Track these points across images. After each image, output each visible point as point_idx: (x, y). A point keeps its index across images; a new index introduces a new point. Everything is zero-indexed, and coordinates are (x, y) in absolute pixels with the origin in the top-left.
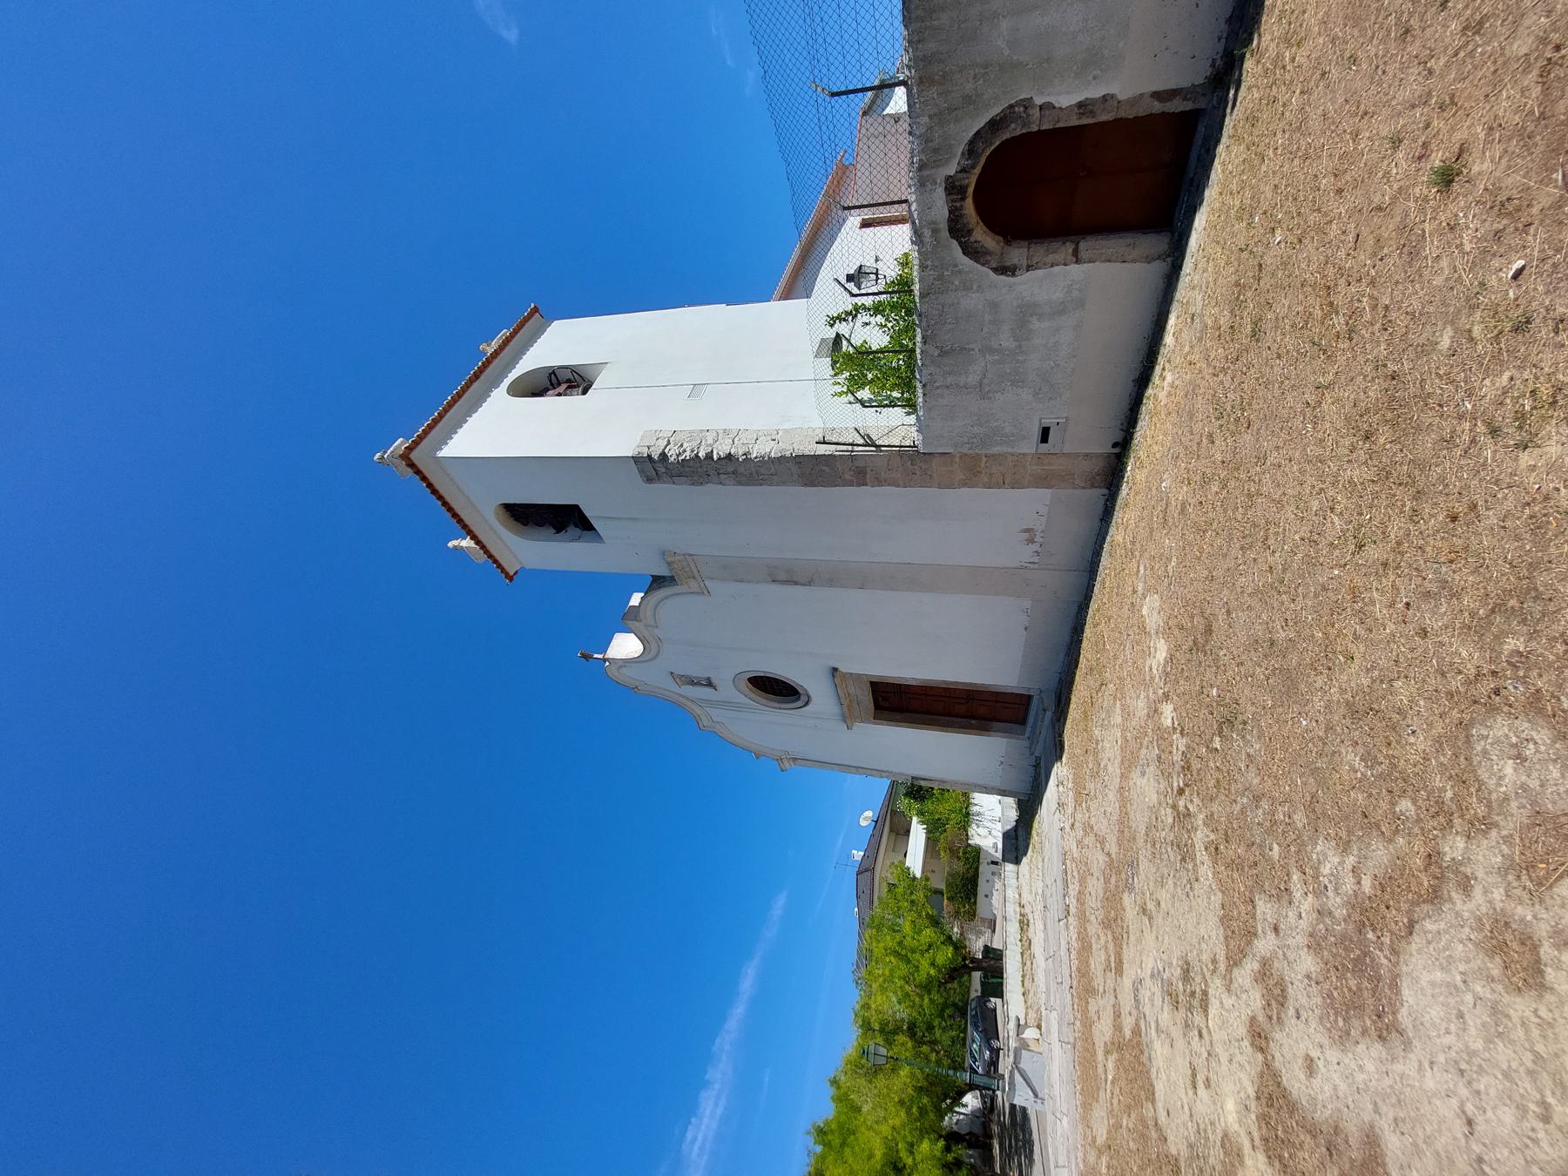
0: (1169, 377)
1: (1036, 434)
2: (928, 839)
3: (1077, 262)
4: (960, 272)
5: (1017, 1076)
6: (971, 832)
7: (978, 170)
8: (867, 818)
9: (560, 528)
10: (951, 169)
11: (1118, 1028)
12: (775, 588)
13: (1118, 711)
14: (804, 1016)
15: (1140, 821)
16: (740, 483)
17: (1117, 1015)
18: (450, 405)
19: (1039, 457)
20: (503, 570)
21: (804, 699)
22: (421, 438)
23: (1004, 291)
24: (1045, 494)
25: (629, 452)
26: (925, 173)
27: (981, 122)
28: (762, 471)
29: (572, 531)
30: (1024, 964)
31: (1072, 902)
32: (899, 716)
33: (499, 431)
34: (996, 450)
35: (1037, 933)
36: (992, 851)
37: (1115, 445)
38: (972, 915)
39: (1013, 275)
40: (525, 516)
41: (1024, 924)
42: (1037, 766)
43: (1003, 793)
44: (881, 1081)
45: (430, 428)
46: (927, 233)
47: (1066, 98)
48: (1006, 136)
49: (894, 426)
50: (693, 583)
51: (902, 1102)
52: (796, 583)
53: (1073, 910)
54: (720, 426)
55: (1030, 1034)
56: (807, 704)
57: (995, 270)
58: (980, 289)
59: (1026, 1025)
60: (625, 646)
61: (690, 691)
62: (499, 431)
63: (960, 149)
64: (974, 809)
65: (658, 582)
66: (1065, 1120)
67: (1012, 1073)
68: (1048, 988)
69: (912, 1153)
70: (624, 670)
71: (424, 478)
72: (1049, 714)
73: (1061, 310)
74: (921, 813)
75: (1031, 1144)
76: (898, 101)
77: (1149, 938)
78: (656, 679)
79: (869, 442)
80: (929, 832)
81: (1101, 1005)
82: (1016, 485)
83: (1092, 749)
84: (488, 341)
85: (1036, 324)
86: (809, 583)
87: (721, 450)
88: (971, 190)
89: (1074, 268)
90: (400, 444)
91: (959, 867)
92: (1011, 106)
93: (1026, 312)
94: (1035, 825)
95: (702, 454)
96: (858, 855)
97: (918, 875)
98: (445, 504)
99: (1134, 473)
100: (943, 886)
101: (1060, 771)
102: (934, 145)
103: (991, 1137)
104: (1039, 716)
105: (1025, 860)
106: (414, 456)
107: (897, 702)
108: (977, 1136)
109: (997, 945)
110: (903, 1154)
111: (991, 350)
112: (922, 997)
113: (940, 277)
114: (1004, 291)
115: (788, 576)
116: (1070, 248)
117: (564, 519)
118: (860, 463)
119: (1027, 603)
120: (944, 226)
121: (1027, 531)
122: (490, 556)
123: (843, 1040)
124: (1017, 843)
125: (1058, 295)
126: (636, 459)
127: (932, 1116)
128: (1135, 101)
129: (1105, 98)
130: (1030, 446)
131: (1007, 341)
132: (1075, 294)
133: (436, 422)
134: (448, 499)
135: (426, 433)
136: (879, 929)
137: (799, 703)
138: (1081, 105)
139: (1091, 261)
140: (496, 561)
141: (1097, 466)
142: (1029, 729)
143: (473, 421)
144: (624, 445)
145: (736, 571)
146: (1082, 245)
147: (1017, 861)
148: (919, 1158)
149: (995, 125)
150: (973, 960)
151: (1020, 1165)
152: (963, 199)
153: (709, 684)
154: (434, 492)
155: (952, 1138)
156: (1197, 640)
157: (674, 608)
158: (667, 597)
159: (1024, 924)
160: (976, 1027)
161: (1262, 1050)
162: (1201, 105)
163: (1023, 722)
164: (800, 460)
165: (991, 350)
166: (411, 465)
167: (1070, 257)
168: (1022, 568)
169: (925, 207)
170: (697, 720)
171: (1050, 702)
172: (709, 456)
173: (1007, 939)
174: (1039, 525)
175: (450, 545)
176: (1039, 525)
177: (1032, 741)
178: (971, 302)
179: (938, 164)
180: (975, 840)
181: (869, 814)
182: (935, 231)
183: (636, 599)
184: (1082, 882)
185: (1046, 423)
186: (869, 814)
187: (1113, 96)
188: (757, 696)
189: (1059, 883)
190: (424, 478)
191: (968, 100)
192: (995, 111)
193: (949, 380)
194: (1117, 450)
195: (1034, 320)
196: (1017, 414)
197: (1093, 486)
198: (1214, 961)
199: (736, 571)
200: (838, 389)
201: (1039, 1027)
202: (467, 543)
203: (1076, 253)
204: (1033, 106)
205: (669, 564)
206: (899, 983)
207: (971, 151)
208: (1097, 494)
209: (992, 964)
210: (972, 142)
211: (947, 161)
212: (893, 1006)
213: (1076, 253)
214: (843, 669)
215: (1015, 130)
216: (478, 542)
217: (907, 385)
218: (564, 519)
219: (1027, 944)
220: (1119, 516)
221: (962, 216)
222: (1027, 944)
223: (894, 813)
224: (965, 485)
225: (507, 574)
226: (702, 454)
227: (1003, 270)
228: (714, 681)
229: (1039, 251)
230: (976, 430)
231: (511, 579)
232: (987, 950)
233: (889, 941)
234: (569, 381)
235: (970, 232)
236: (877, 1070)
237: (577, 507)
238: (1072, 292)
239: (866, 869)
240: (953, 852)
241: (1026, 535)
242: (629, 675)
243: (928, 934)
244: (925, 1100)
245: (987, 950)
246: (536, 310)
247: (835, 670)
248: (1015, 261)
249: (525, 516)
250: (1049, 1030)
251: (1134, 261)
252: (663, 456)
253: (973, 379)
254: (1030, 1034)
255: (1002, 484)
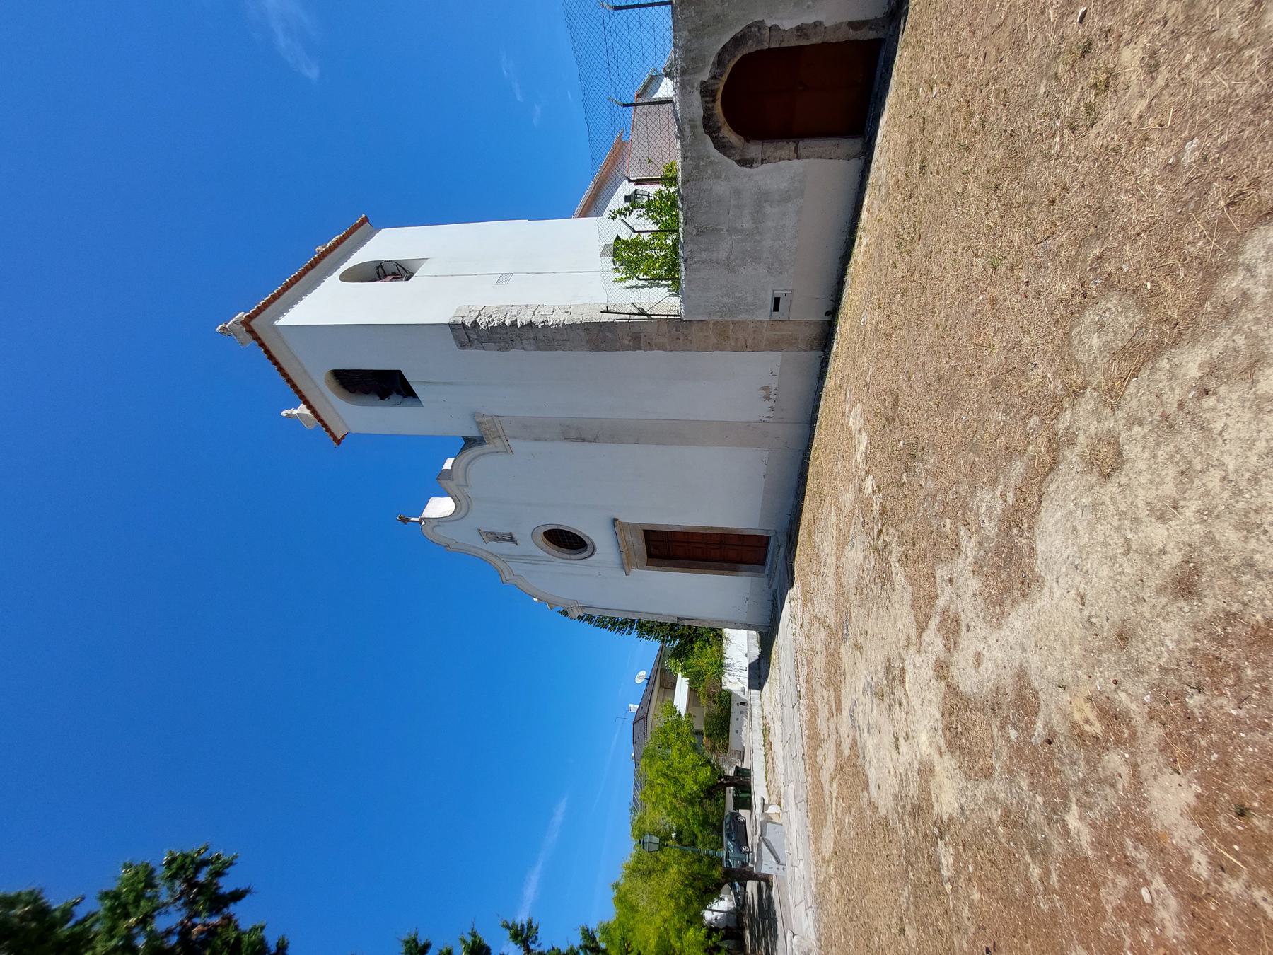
0: (864, 241)
1: (770, 304)
2: (691, 690)
3: (798, 157)
4: (712, 162)
5: (764, 847)
6: (724, 680)
7: (725, 78)
8: (641, 677)
9: (383, 395)
10: (705, 76)
11: (839, 754)
12: (567, 445)
13: (834, 513)
14: (588, 851)
15: (850, 582)
16: (539, 349)
17: (839, 744)
18: (288, 286)
19: (773, 323)
20: (332, 434)
21: (590, 549)
22: (260, 310)
23: (745, 180)
24: (775, 357)
25: (446, 320)
26: (686, 78)
27: (726, 39)
28: (558, 337)
29: (395, 398)
30: (767, 763)
31: (803, 688)
32: (667, 562)
33: (330, 304)
34: (741, 317)
35: (776, 738)
36: (741, 694)
37: (827, 314)
38: (726, 748)
39: (752, 167)
40: (355, 382)
41: (766, 731)
42: (774, 600)
43: (748, 627)
44: (654, 881)
45: (269, 302)
46: (687, 128)
47: (788, 24)
48: (746, 51)
49: (660, 300)
50: (498, 442)
51: (671, 896)
52: (583, 440)
53: (803, 692)
54: (523, 303)
55: (772, 810)
56: (592, 554)
57: (738, 162)
58: (727, 178)
59: (769, 804)
60: (440, 507)
61: (495, 547)
62: (330, 304)
63: (712, 59)
64: (726, 662)
65: (469, 442)
66: (801, 866)
67: (759, 845)
68: (785, 770)
69: (680, 938)
70: (437, 529)
71: (262, 345)
72: (782, 550)
73: (786, 199)
74: (684, 669)
75: (775, 921)
76: (666, 89)
77: (861, 665)
78: (465, 537)
79: (642, 313)
80: (691, 683)
81: (828, 750)
82: (756, 348)
83: (816, 558)
84: (323, 244)
85: (769, 209)
86: (595, 440)
87: (524, 319)
88: (719, 94)
89: (796, 162)
90: (241, 315)
91: (715, 708)
92: (749, 26)
93: (762, 198)
94: (773, 656)
95: (507, 322)
96: (634, 707)
97: (683, 712)
98: (280, 369)
99: (843, 328)
100: (702, 728)
101: (794, 592)
102: (691, 55)
103: (743, 929)
104: (775, 554)
105: (766, 686)
106: (254, 323)
107: (668, 548)
108: (732, 929)
109: (745, 766)
110: (673, 941)
111: (736, 231)
112: (687, 809)
113: (697, 167)
114: (745, 180)
115: (577, 434)
116: (792, 146)
117: (386, 385)
118: (636, 330)
119: (766, 453)
120: (700, 123)
121: (764, 389)
122: (320, 420)
123: (622, 849)
124: (759, 673)
125: (784, 185)
126: (452, 326)
127: (696, 904)
128: (837, 27)
129: (816, 24)
130: (765, 314)
131: (748, 225)
132: (797, 184)
133: (275, 298)
134: (283, 365)
135: (265, 306)
136: (652, 757)
137: (587, 554)
138: (798, 29)
139: (808, 157)
140: (325, 425)
141: (811, 332)
142: (768, 567)
143: (308, 299)
144: (442, 313)
145: (534, 430)
146: (801, 144)
147: (760, 688)
148: (686, 944)
149: (737, 41)
150: (727, 778)
151: (767, 944)
152: (714, 101)
153: (512, 539)
154: (271, 357)
155: (712, 930)
156: (888, 417)
157: (483, 464)
158: (475, 458)
159: (766, 731)
160: (730, 838)
161: (945, 677)
162: (881, 35)
163: (763, 564)
164: (589, 327)
165: (736, 231)
166: (251, 331)
167: (793, 154)
168: (761, 421)
169: (686, 105)
170: (500, 573)
171: (783, 539)
172: (514, 324)
173: (756, 765)
174: (773, 383)
175: (284, 413)
176: (773, 383)
177: (770, 576)
178: (720, 188)
179: (696, 71)
180: (727, 686)
181: (643, 673)
182: (693, 127)
183: (448, 465)
184: (810, 662)
185: (777, 294)
186: (643, 673)
187: (821, 23)
188: (551, 549)
189: (793, 678)
190: (262, 345)
191: (717, 18)
192: (738, 29)
193: (704, 256)
194: (828, 318)
195: (767, 205)
196: (756, 285)
197: (812, 349)
198: (908, 639)
199: (534, 430)
200: (618, 276)
201: (780, 804)
202: (302, 409)
203: (796, 150)
204: (764, 27)
205: (479, 424)
206: (669, 799)
207: (720, 62)
208: (816, 354)
209: (742, 782)
210: (720, 54)
211: (701, 69)
212: (660, 817)
213: (796, 150)
214: (622, 519)
215: (750, 47)
216: (314, 411)
217: (673, 268)
218: (386, 385)
219: (768, 746)
220: (831, 368)
221: (713, 115)
222: (768, 746)
223: (663, 671)
224: (717, 349)
225: (335, 439)
226: (507, 322)
227: (746, 162)
228: (516, 536)
229: (770, 149)
230: (725, 300)
231: (339, 442)
232: (738, 770)
233: (660, 765)
234: (394, 274)
235: (719, 129)
236: (649, 873)
237: (400, 372)
238: (792, 178)
239: (641, 718)
240: (710, 697)
241: (763, 393)
242: (442, 535)
243: (692, 757)
244: (690, 892)
245: (738, 770)
246: (366, 220)
247: (616, 520)
248: (753, 155)
249: (355, 382)
250: (787, 802)
251: (838, 158)
252: (475, 324)
253: (722, 255)
254: (772, 810)
255: (744, 348)
